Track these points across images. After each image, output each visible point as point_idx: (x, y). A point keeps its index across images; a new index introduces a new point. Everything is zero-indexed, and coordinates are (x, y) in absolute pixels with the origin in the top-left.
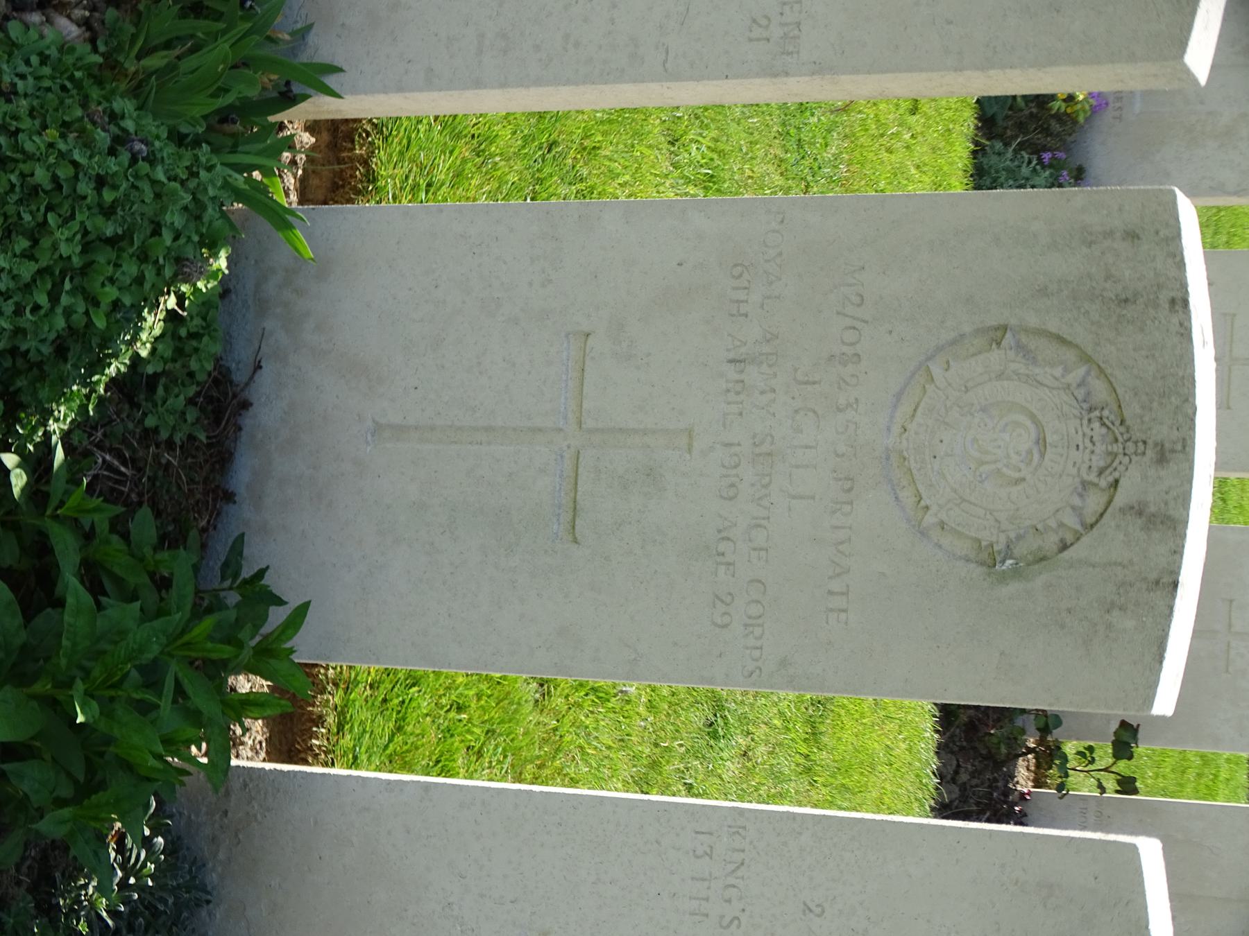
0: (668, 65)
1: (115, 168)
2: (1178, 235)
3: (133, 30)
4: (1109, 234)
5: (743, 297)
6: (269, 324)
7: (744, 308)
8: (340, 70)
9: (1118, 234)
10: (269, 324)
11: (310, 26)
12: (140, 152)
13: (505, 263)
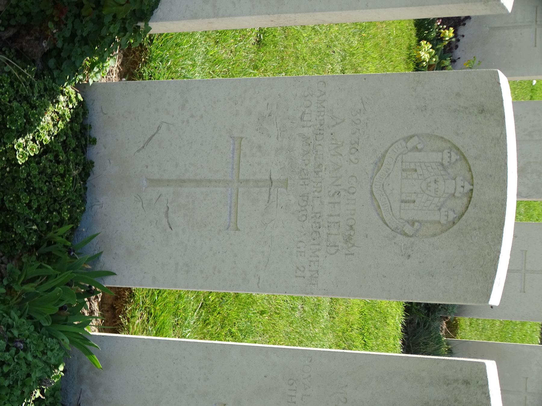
0: (260, 285)
1: (8, 357)
2: (487, 384)
3: (19, 273)
4: (456, 381)
5: (293, 394)
6: (83, 387)
7: (294, 399)
8: (114, 274)
9: (460, 381)
10: (83, 387)
11: (102, 253)
12: (20, 347)
13: (188, 369)
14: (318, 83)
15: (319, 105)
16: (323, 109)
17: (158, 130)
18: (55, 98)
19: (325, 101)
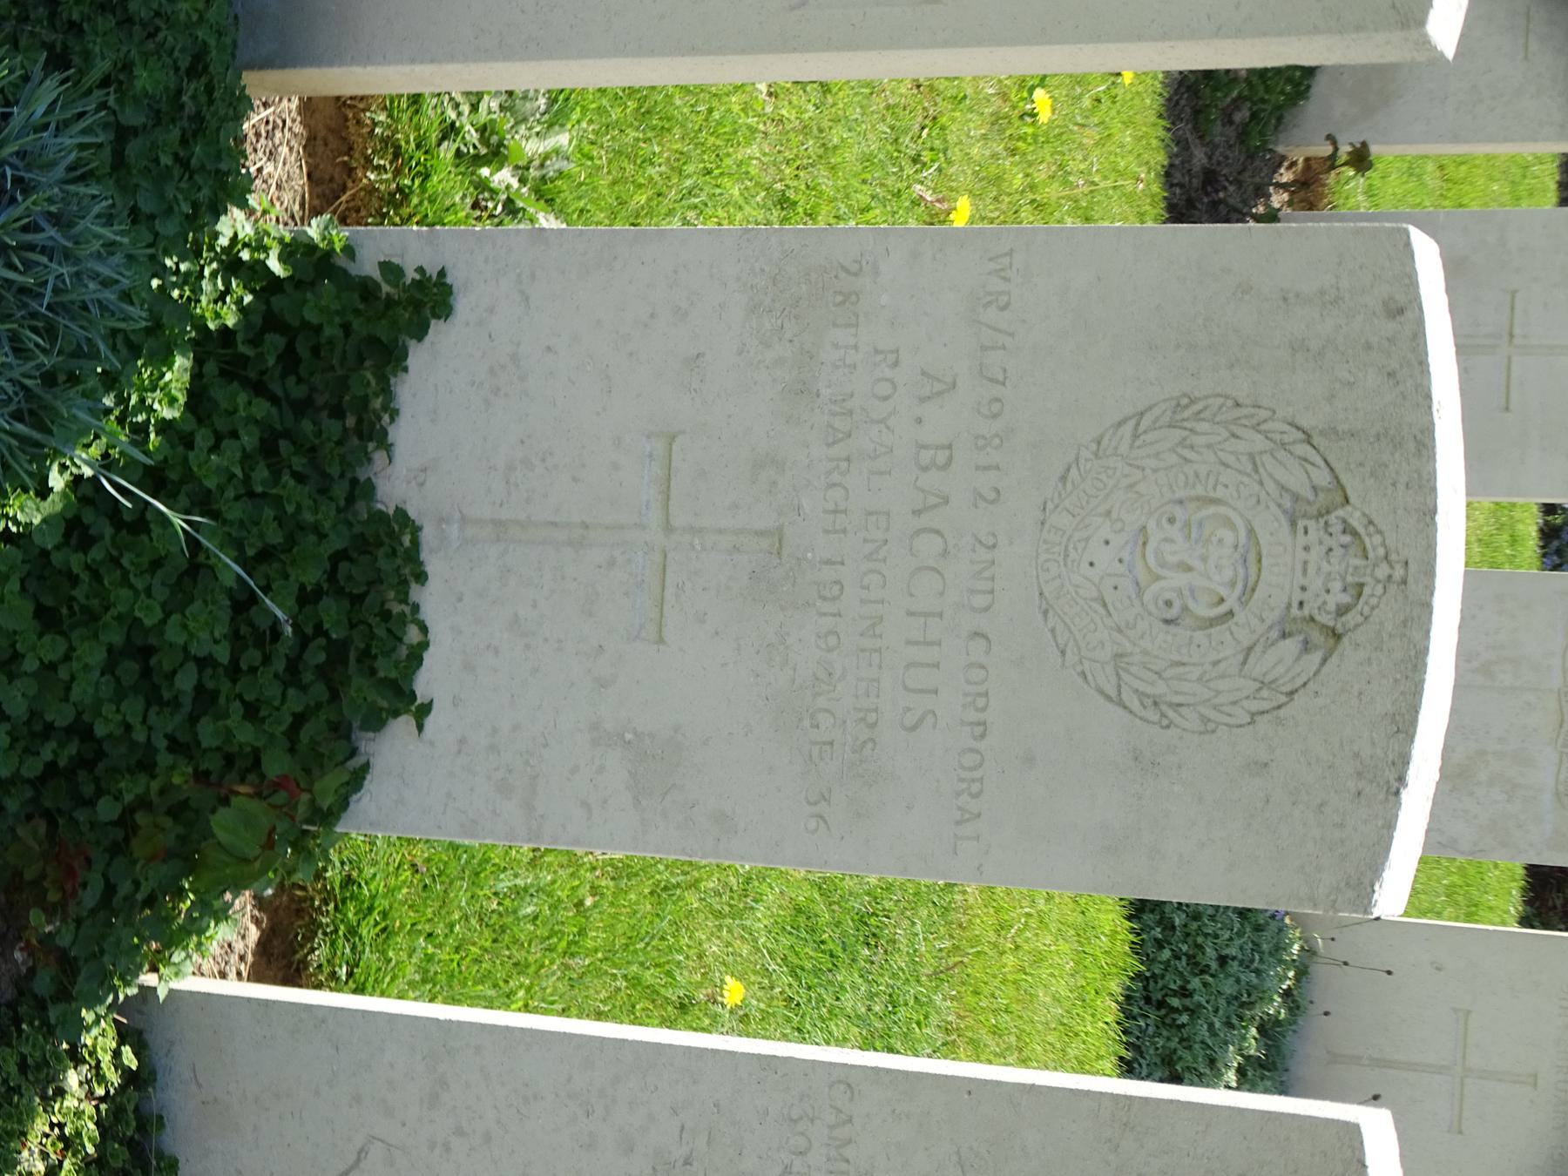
14: (831, 1086)
15: (833, 1153)
16: (844, 1166)
17: (358, 1160)
18: (51, 1079)
19: (850, 1141)
